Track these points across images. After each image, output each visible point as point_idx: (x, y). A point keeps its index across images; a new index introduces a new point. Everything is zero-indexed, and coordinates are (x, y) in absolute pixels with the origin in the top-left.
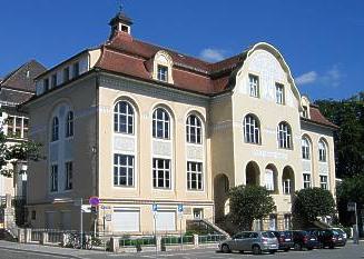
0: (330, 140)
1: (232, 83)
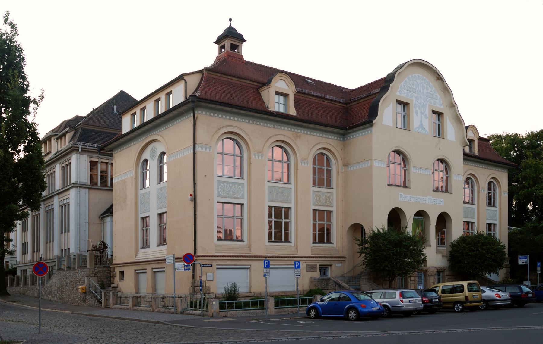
0: (503, 177)
1: (373, 112)
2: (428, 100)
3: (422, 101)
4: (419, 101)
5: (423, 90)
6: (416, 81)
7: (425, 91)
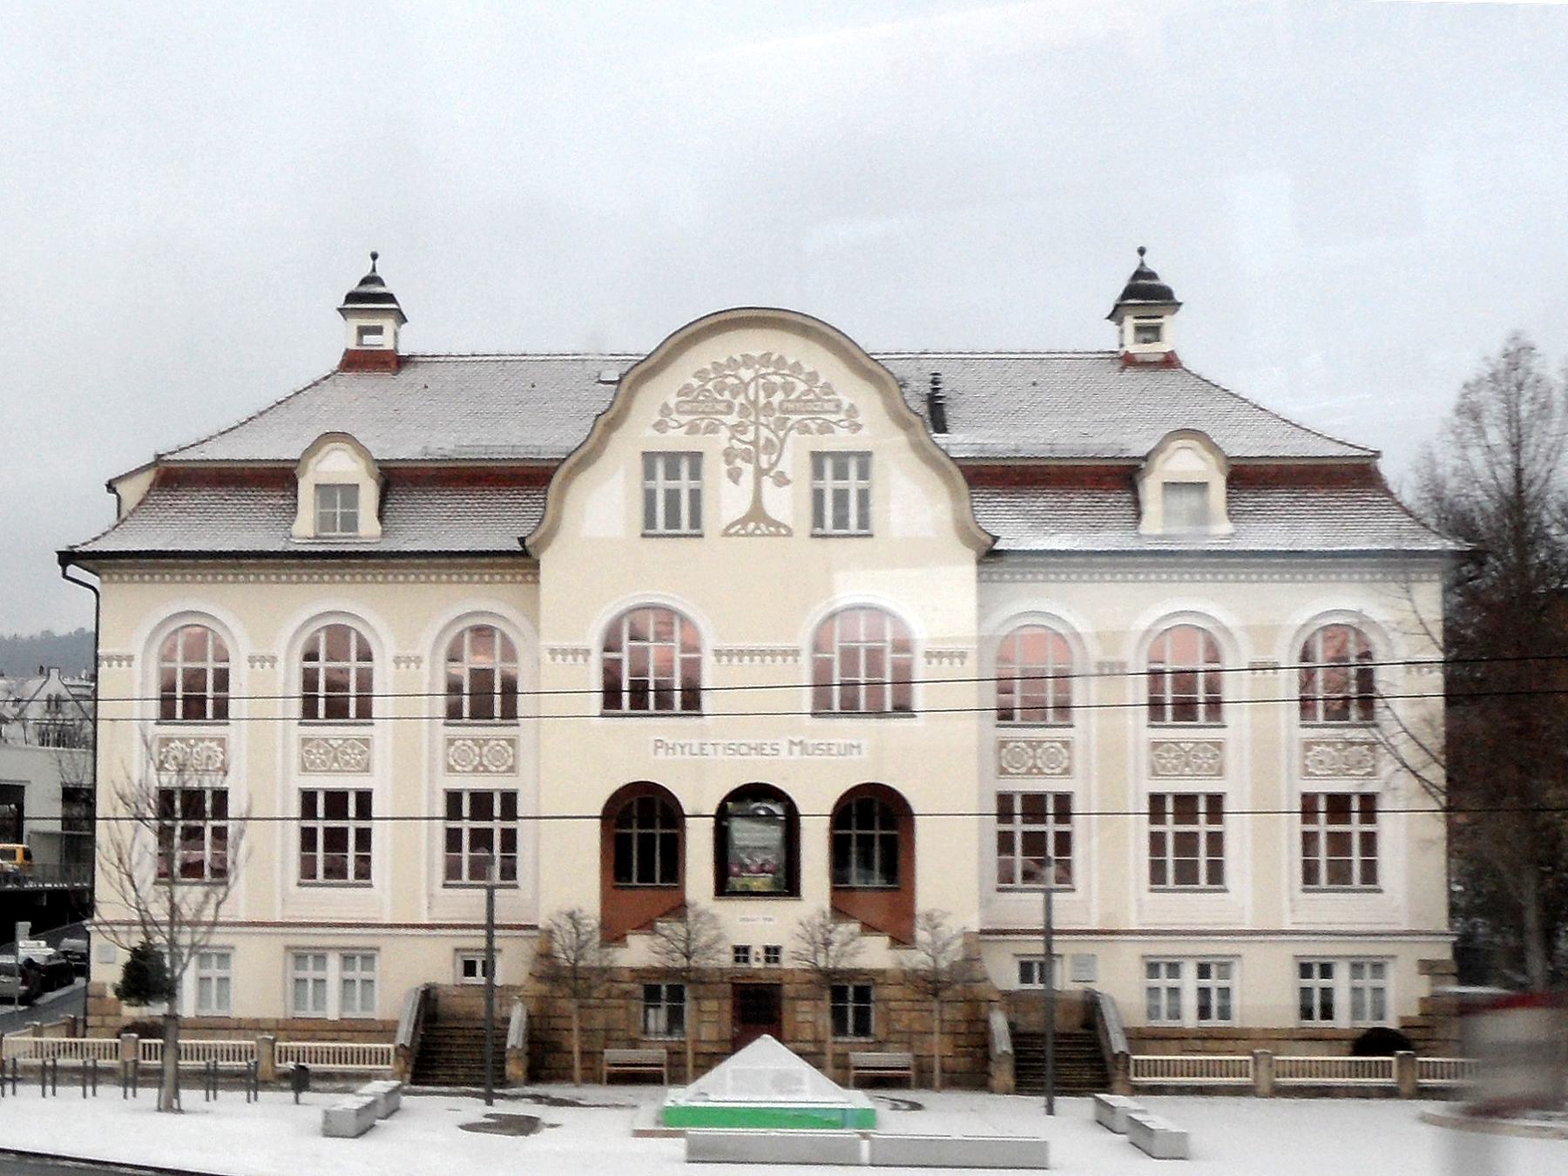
2: (789, 424)
3: (764, 432)
4: (750, 436)
5: (769, 396)
6: (736, 377)
7: (778, 397)
